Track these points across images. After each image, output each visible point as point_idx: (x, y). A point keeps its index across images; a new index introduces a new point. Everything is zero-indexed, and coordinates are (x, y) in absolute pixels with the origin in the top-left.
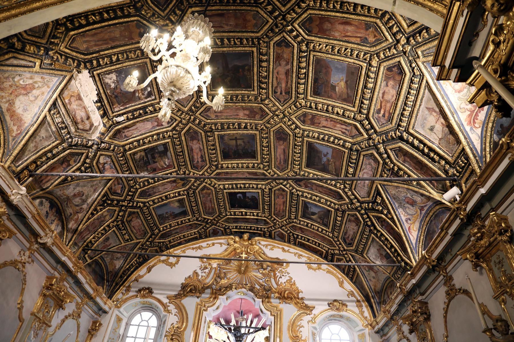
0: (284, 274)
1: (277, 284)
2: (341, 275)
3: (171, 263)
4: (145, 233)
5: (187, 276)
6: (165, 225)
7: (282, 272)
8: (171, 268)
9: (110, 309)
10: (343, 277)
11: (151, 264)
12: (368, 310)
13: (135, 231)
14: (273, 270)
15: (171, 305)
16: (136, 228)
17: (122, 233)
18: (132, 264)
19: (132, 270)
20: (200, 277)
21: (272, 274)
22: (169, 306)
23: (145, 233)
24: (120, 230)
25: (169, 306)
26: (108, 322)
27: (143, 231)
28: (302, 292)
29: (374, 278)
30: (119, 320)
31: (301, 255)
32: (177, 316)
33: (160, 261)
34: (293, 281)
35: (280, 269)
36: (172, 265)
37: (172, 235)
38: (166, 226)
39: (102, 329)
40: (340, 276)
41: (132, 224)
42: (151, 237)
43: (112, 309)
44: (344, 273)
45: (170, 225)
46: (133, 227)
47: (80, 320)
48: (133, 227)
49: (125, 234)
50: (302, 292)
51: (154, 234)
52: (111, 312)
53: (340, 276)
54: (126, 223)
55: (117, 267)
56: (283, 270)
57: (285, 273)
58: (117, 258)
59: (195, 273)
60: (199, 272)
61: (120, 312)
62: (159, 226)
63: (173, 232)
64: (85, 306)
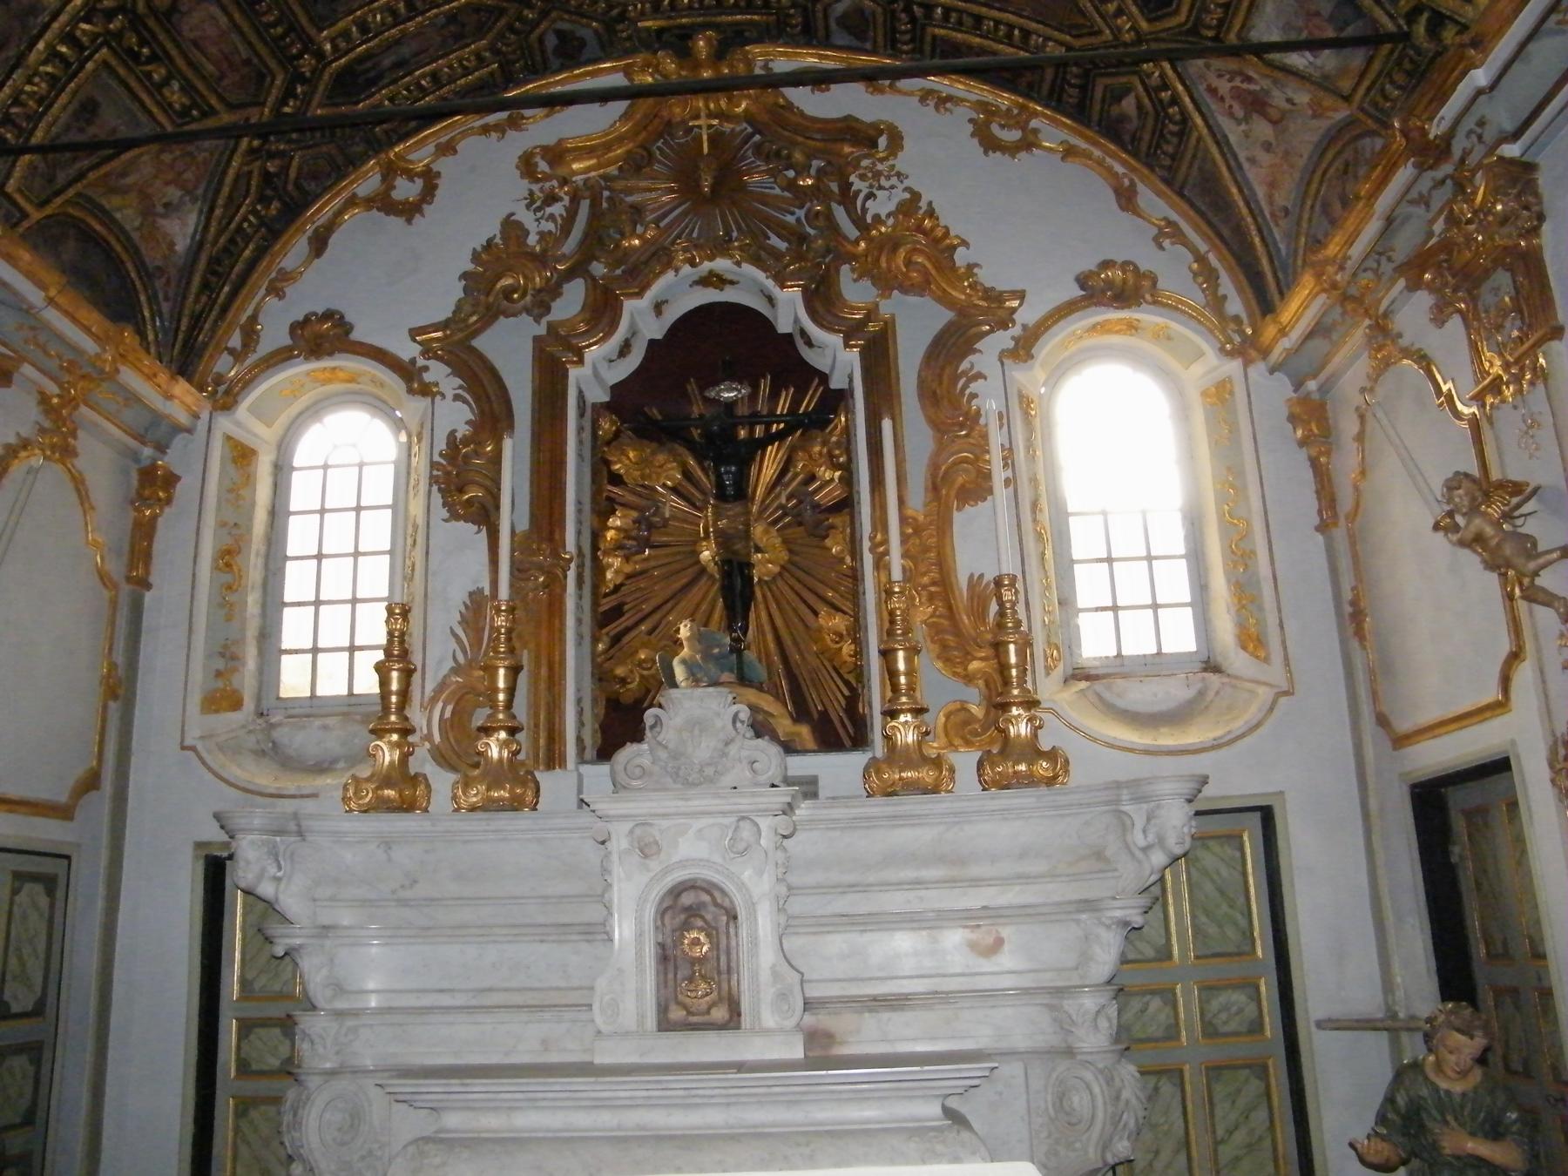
0: (883, 182)
1: (859, 221)
2: (1124, 163)
3: (406, 202)
4: (261, 78)
5: (479, 242)
6: (341, 25)
7: (877, 175)
8: (409, 221)
9: (196, 416)
10: (1133, 170)
11: (322, 220)
12: (1240, 291)
13: (210, 68)
14: (840, 171)
15: (432, 363)
16: (213, 50)
17: (149, 75)
18: (239, 229)
19: (247, 253)
20: (532, 240)
21: (834, 187)
22: (426, 369)
23: (261, 77)
24: (136, 57)
25: (426, 369)
26: (201, 470)
27: (247, 62)
28: (964, 243)
29: (1267, 147)
30: (243, 455)
31: (949, 98)
32: (465, 401)
33: (352, 202)
34: (923, 204)
35: (865, 163)
36: (408, 211)
37: (380, 76)
38: (346, 34)
39: (185, 490)
40: (1119, 169)
41: (185, 28)
42: (289, 93)
43: (205, 415)
44: (1135, 154)
45: (364, 28)
46: (195, 43)
47: (80, 463)
48: (195, 43)
49: (166, 82)
50: (964, 243)
51: (301, 79)
52: (202, 426)
53: (1119, 169)
54: (151, 23)
55: (181, 245)
56: (880, 167)
57: (888, 178)
58: (166, 205)
59: (511, 227)
60: (527, 218)
61: (238, 424)
62: (312, 31)
63: (387, 62)
64: (83, 409)
